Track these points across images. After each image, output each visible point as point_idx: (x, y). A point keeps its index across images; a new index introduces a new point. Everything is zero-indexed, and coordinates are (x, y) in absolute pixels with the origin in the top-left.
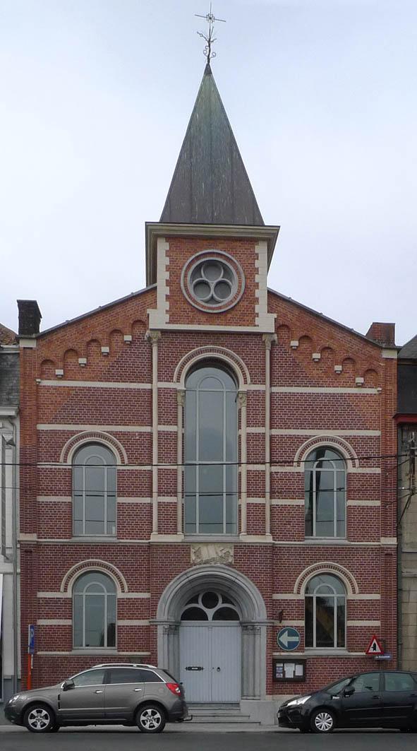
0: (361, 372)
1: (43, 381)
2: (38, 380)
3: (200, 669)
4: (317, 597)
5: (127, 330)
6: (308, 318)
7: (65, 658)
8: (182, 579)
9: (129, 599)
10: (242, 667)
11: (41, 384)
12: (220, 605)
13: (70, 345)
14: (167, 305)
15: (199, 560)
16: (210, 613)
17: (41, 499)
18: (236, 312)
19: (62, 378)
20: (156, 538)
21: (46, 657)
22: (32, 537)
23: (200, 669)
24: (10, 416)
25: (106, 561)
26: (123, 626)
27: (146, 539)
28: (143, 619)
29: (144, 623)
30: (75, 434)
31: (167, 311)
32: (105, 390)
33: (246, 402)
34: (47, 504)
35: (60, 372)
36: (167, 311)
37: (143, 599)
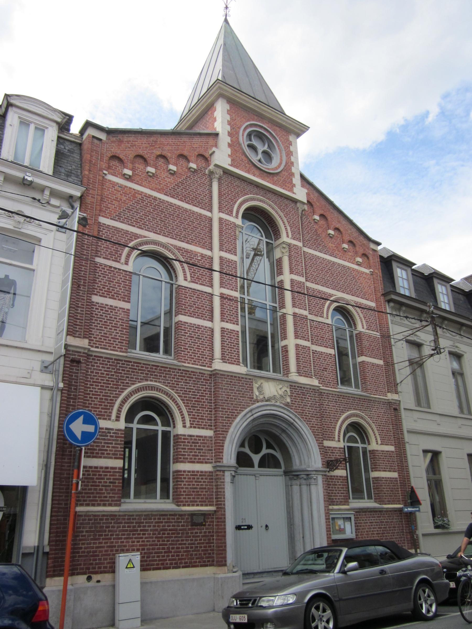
0: (360, 254)
1: (108, 175)
2: (105, 172)
3: (249, 527)
4: (162, 431)
5: (193, 158)
6: (323, 202)
7: (113, 516)
8: (248, 416)
9: (190, 436)
10: (313, 529)
11: (106, 177)
12: (265, 451)
13: (141, 152)
14: (229, 151)
15: (261, 397)
16: (256, 458)
17: (96, 299)
18: (280, 178)
19: (129, 178)
20: (218, 365)
21: (87, 515)
22: (84, 343)
23: (249, 527)
24: (71, 197)
25: (167, 386)
26: (184, 471)
27: (208, 367)
28: (206, 463)
29: (207, 468)
30: (139, 238)
31: (229, 155)
32: (171, 205)
33: (288, 252)
34: (102, 306)
35: (128, 172)
36: (229, 155)
37: (205, 437)
